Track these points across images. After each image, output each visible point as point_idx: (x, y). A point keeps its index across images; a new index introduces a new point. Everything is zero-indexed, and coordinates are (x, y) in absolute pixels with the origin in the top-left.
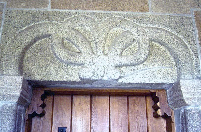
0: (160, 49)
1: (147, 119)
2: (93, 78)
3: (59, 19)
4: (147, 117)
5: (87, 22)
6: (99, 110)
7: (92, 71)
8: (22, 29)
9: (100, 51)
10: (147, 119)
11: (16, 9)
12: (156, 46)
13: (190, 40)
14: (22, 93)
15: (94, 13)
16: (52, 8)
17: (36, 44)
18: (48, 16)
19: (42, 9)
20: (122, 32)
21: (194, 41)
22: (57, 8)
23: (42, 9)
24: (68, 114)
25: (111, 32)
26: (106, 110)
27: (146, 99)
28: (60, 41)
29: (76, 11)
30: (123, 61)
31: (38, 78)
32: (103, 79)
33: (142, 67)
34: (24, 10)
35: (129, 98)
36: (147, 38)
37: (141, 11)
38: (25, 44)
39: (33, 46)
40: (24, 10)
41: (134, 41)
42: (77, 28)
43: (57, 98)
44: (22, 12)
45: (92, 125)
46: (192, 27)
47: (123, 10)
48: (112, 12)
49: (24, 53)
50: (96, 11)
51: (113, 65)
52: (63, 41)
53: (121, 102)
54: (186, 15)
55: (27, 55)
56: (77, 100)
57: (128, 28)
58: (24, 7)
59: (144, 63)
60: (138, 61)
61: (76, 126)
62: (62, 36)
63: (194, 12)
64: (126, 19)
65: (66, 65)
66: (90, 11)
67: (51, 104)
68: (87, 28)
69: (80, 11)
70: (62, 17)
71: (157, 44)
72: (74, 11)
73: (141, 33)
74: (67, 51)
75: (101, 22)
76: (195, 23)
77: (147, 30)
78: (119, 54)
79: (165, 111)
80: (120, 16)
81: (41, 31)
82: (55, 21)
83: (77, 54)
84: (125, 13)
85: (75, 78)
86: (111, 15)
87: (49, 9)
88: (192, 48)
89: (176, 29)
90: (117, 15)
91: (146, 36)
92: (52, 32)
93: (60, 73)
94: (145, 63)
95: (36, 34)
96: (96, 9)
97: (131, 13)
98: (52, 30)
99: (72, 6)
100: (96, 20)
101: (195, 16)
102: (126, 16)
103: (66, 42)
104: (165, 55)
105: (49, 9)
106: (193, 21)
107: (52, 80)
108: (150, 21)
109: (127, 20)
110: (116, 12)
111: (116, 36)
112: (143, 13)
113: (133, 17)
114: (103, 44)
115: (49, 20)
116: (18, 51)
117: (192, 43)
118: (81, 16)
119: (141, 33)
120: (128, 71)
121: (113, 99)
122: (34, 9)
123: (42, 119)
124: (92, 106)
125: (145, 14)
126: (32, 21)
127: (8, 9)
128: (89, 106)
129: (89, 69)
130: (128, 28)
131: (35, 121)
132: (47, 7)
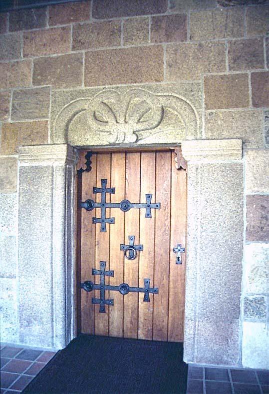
0: (173, 114)
1: (171, 171)
2: (117, 142)
3: (90, 95)
4: (171, 169)
5: (112, 95)
6: (132, 165)
7: (116, 137)
8: (65, 107)
9: (121, 120)
10: (171, 171)
11: (59, 90)
12: (169, 111)
13: (197, 105)
14: (67, 156)
15: (118, 87)
16: (85, 86)
17: (76, 116)
18: (83, 93)
19: (78, 88)
20: (140, 101)
21: (200, 105)
22: (89, 86)
23: (78, 88)
24: (108, 168)
25: (132, 102)
26: (138, 165)
27: (156, 154)
28: (92, 114)
29: (104, 86)
30: (139, 127)
31: (79, 144)
32: (124, 142)
33: (156, 130)
34: (65, 90)
35: (142, 154)
36: (160, 106)
37: (157, 81)
38: (68, 118)
39: (74, 119)
40: (65, 90)
41: (150, 109)
42: (104, 101)
43: (100, 156)
44: (64, 92)
45: (127, 177)
46: (200, 93)
47: (141, 82)
48: (132, 84)
49: (67, 125)
50: (118, 85)
51: (132, 131)
52: (95, 113)
53: (150, 157)
54: (196, 81)
55: (70, 126)
56: (115, 157)
57: (144, 98)
58: (65, 88)
59: (158, 127)
60: (151, 126)
61: (114, 177)
62: (93, 110)
63: (204, 77)
64: (143, 89)
65: (98, 132)
66: (114, 86)
67: (95, 161)
68: (113, 101)
69: (107, 87)
70: (93, 93)
71: (171, 110)
72: (102, 87)
73: (155, 101)
74: (98, 122)
75: (123, 95)
76: (203, 89)
77: (160, 98)
78: (136, 121)
79: (181, 165)
80: (139, 87)
81: (78, 107)
82: (88, 97)
83: (105, 124)
84: (142, 84)
85: (105, 143)
86: (131, 87)
87: (83, 87)
88: (198, 112)
89: (185, 96)
90: (136, 86)
91: (159, 104)
92: (86, 107)
93: (94, 139)
94: (159, 127)
95: (75, 110)
96: (119, 83)
97: (148, 83)
98: (86, 106)
99: (100, 83)
100: (119, 93)
101: (204, 81)
102: (144, 87)
103: (97, 113)
104: (177, 119)
105: (83, 87)
106: (202, 86)
107: (89, 144)
108: (163, 90)
109: (144, 91)
110: (135, 85)
111: (136, 105)
112: (158, 83)
113: (150, 88)
114: (124, 114)
115: (84, 97)
116: (63, 125)
117: (198, 107)
118: (108, 91)
119: (155, 101)
120: (145, 134)
121: (143, 155)
122: (72, 89)
123: (89, 173)
124: (127, 161)
125: (160, 83)
126: (72, 99)
127: (53, 90)
128: (124, 162)
129: (113, 136)
130: (144, 98)
131: (84, 175)
132: (81, 85)
